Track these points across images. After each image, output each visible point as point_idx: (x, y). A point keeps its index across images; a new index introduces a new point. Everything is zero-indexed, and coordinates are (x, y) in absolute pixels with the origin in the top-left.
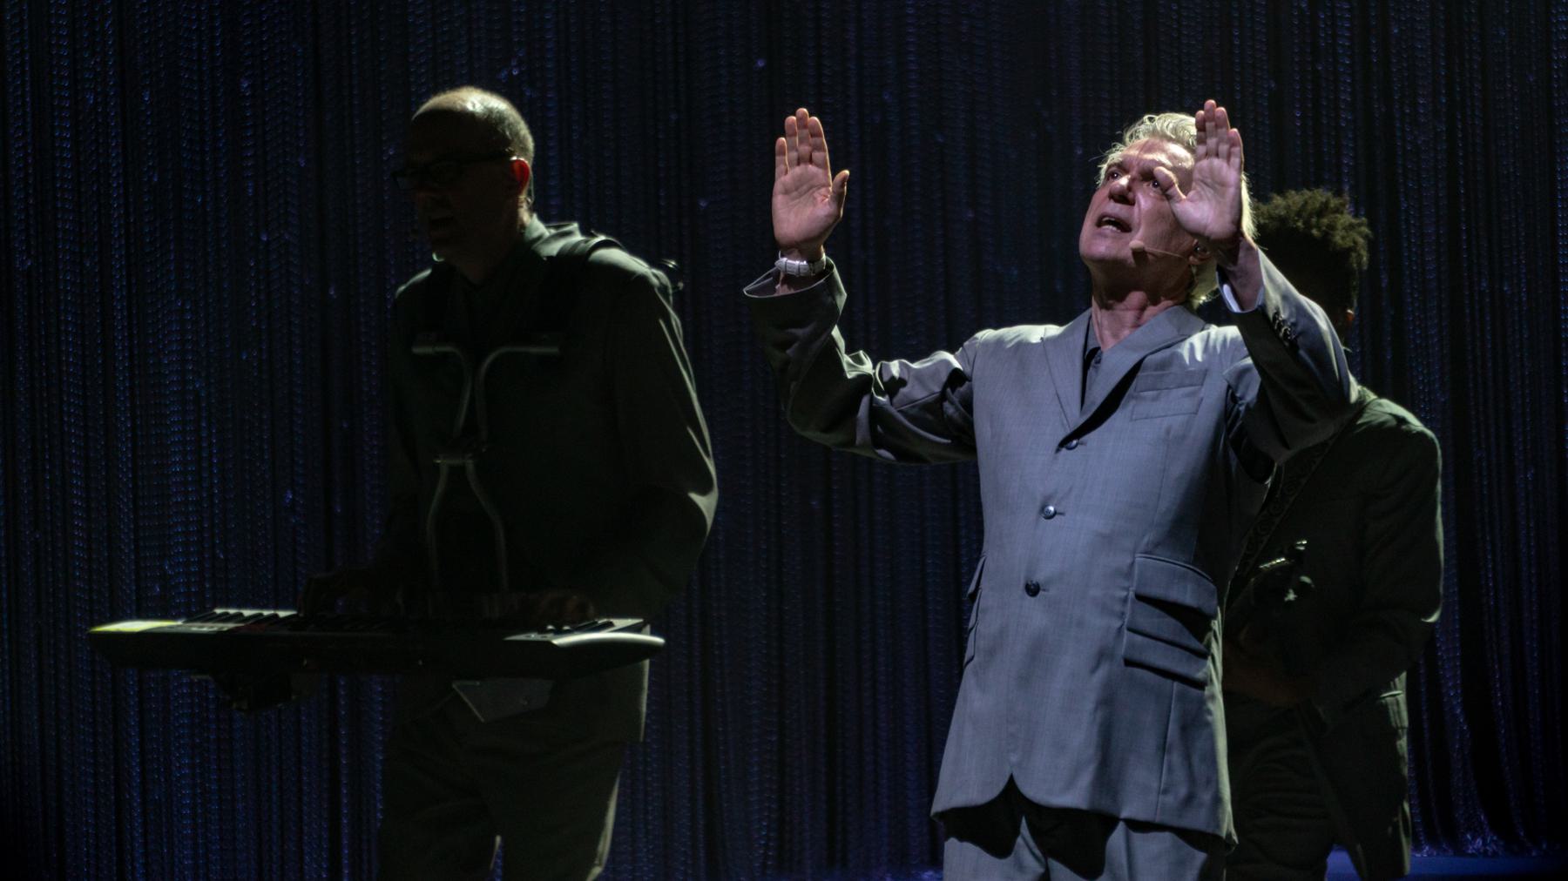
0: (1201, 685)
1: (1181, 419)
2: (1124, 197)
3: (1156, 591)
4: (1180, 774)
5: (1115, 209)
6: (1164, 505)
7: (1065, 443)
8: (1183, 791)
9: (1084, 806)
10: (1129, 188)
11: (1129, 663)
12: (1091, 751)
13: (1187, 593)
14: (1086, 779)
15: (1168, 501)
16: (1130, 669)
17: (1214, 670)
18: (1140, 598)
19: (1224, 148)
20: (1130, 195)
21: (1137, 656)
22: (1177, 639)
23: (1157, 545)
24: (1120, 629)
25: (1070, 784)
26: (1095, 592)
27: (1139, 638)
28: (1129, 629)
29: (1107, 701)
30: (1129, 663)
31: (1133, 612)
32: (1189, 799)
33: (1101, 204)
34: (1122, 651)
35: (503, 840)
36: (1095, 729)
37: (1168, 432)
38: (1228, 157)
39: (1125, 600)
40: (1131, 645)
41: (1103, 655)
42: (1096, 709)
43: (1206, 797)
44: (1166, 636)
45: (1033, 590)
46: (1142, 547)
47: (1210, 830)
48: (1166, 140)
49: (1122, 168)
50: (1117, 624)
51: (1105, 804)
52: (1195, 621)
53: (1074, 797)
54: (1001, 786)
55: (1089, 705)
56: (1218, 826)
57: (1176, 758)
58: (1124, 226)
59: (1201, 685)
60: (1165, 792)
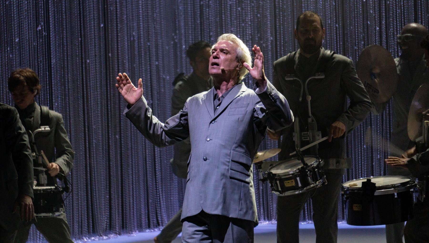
0: (248, 183)
1: (242, 116)
2: (216, 57)
4: (244, 206)
6: (238, 138)
7: (211, 122)
8: (245, 210)
9: (220, 214)
10: (217, 55)
11: (231, 178)
12: (222, 200)
13: (243, 160)
14: (220, 207)
15: (239, 137)
16: (231, 180)
17: (251, 180)
18: (232, 161)
19: (259, 57)
20: (218, 56)
21: (233, 176)
22: (242, 172)
24: (228, 170)
25: (217, 208)
26: (222, 160)
27: (233, 171)
28: (231, 169)
29: (224, 187)
30: (231, 178)
31: (231, 164)
32: (246, 212)
33: (212, 60)
34: (229, 175)
35: (299, 99)
36: (222, 194)
37: (239, 119)
38: (260, 59)
40: (231, 173)
41: (223, 175)
42: (222, 189)
43: (251, 212)
44: (240, 171)
45: (205, 160)
46: (232, 149)
47: (252, 220)
48: (227, 39)
49: (215, 50)
50: (227, 168)
51: (225, 214)
52: (248, 167)
53: (218, 212)
54: (201, 210)
55: (221, 189)
56: (254, 219)
58: (217, 64)
59: (248, 183)
60: (240, 210)
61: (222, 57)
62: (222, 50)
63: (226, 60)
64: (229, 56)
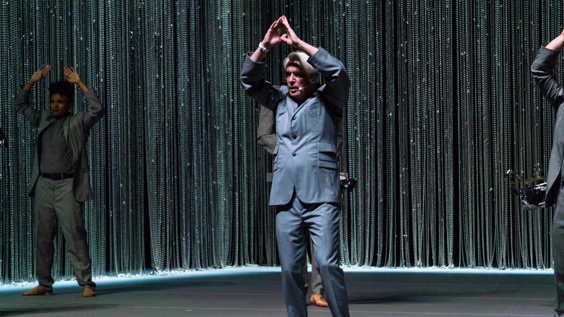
3: (323, 150)
14: (316, 196)
18: (320, 152)
23: (321, 139)
25: (313, 198)
26: (310, 153)
27: (322, 162)
30: (320, 167)
39: (316, 154)
40: (320, 164)
57: (334, 187)
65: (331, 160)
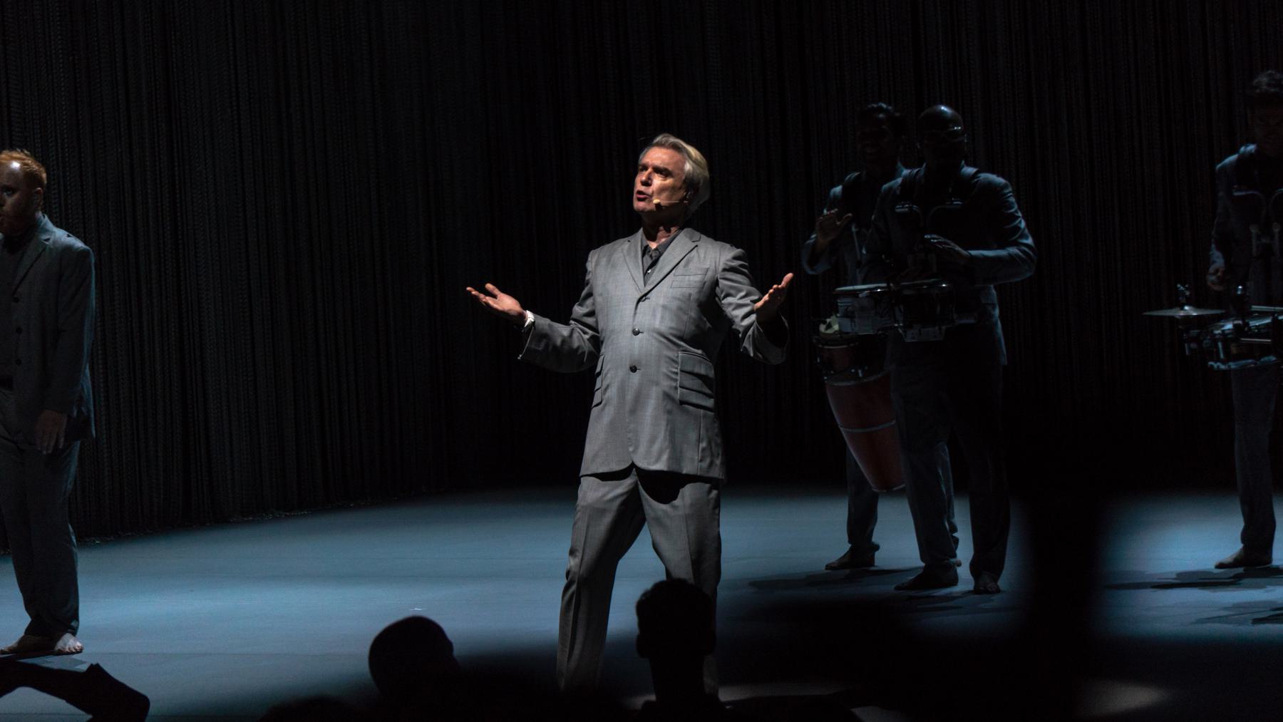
3: (688, 368)
5: (643, 188)
14: (665, 457)
25: (658, 460)
40: (682, 394)
61: (658, 181)
62: (657, 170)
63: (662, 190)
64: (669, 181)
65: (708, 391)
